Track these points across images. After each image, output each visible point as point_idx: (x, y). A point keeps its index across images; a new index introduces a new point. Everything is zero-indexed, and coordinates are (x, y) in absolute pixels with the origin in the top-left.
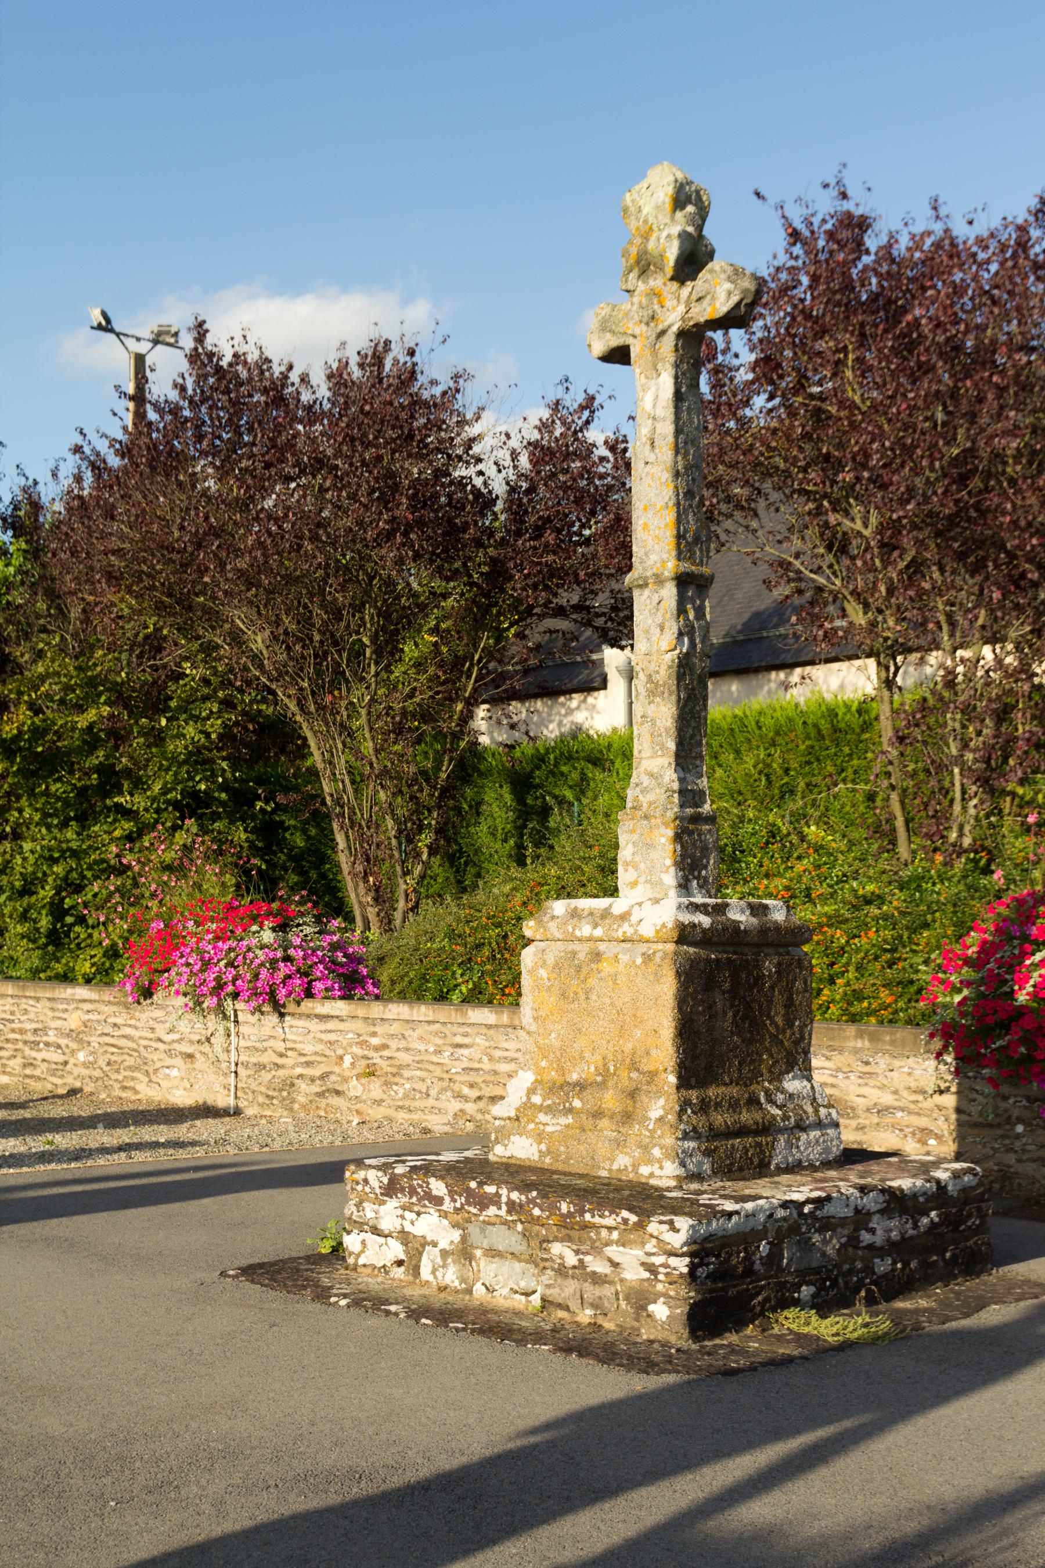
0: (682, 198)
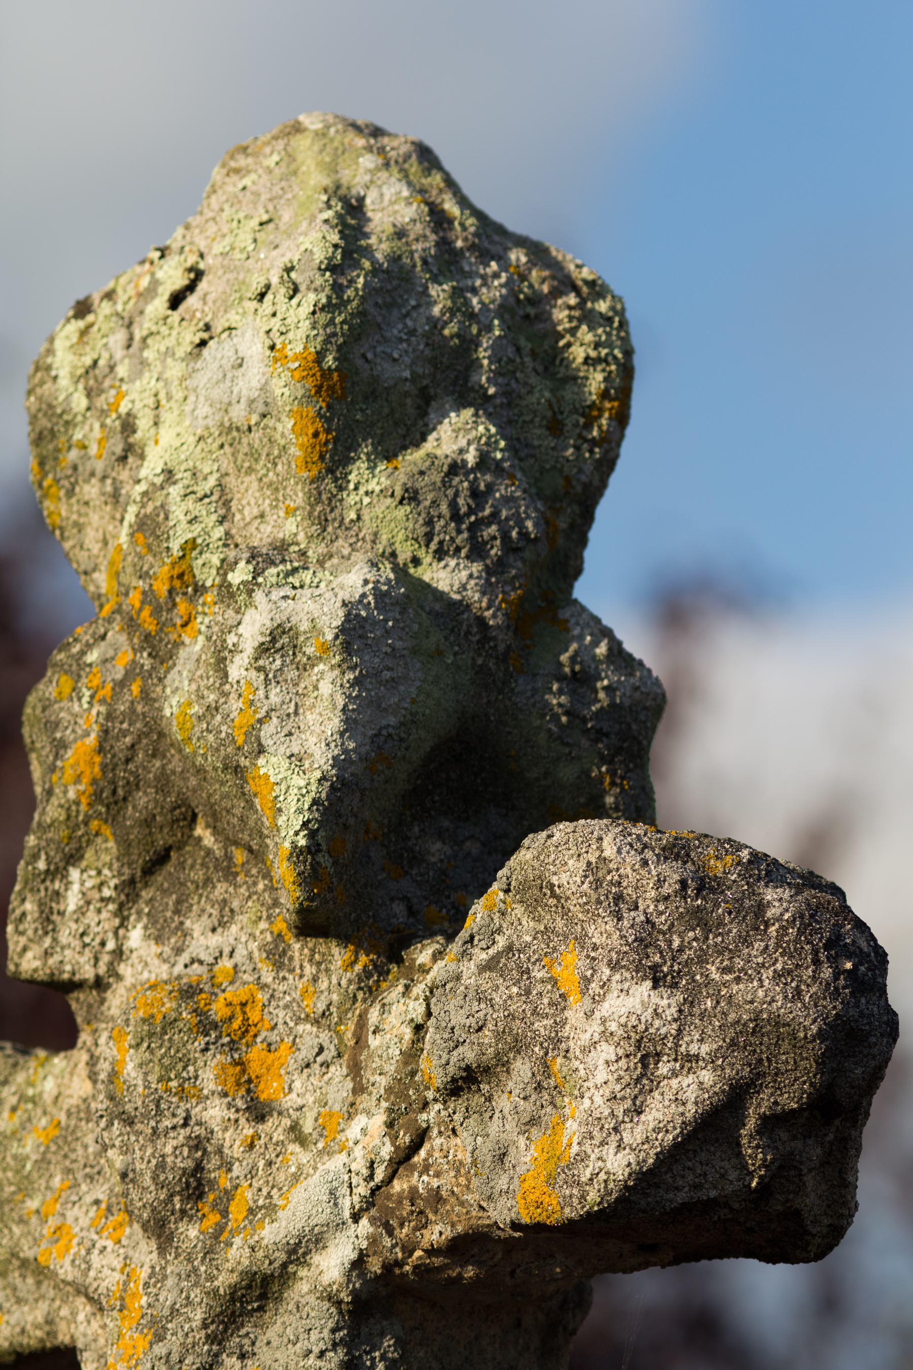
0: (397, 367)
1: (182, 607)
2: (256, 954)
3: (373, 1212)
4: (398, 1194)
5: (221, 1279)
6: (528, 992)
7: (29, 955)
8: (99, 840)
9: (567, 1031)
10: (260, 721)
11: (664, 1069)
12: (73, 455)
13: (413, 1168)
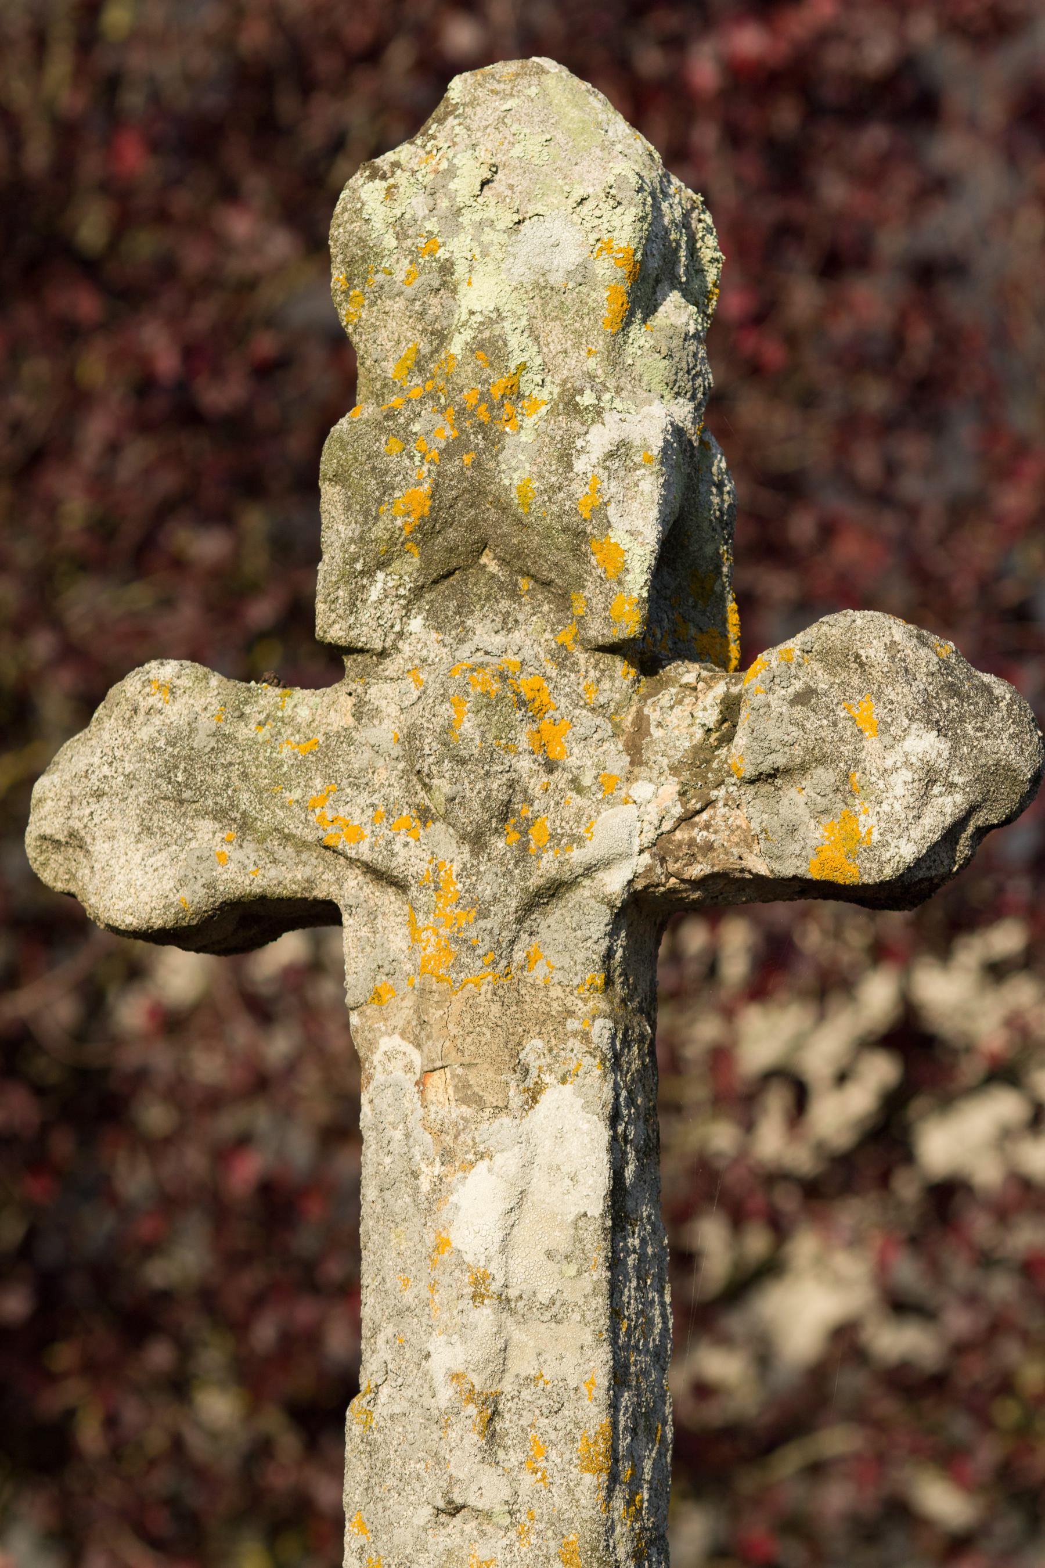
1: (508, 407)
2: (542, 655)
3: (654, 849)
4: (679, 841)
5: (532, 880)
6: (835, 724)
7: (337, 626)
8: (408, 556)
9: (863, 755)
10: (605, 504)
11: (936, 790)
12: (380, 277)
13: (696, 825)
